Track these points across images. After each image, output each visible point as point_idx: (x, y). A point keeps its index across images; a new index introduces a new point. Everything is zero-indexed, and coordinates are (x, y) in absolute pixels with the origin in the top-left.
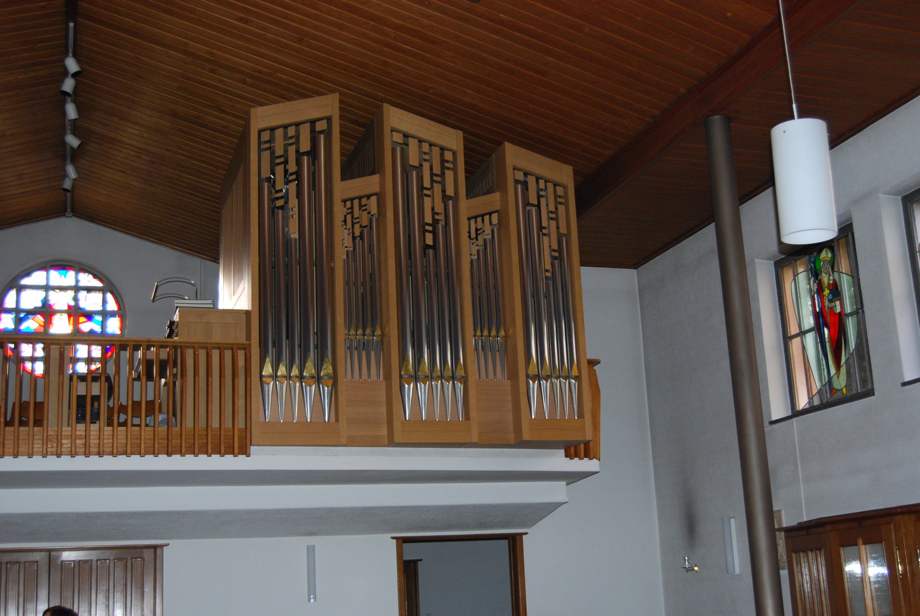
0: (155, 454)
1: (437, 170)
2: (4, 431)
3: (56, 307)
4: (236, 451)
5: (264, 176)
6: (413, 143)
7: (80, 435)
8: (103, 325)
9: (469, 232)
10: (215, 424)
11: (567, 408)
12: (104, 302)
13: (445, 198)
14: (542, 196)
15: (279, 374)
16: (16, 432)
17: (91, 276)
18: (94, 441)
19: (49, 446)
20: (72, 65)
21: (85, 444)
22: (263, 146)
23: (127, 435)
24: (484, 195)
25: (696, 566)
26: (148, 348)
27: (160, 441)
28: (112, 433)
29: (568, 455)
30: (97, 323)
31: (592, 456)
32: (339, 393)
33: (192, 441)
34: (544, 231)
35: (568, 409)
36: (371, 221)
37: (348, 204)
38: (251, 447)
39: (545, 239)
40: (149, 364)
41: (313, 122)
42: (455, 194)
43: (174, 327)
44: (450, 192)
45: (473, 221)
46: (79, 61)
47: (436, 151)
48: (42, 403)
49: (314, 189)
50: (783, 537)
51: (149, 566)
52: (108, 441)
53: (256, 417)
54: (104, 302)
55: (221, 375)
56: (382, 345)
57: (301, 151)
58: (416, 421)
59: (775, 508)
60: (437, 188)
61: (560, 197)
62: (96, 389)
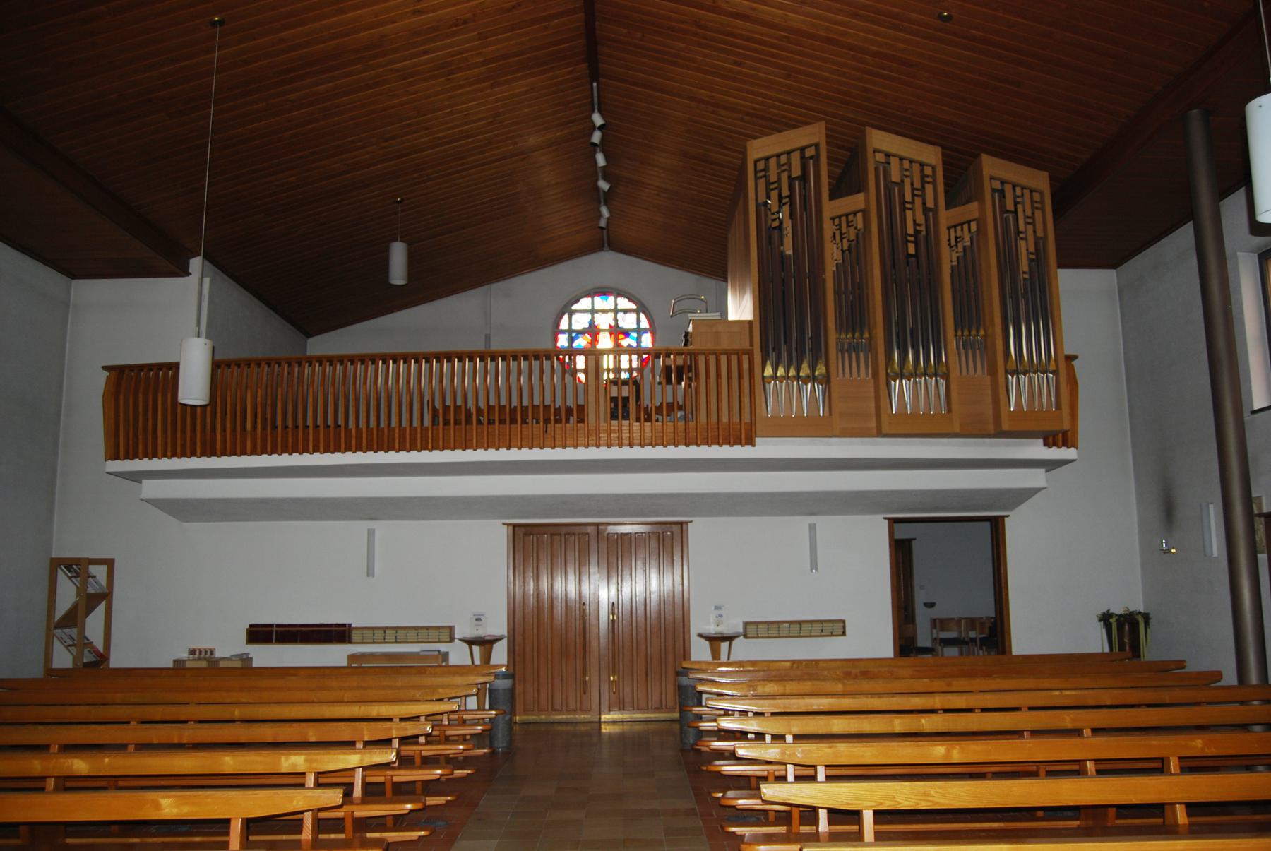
0: (676, 445)
1: (917, 185)
2: (554, 426)
3: (601, 328)
4: (743, 442)
5: (760, 201)
6: (895, 162)
7: (614, 430)
8: (639, 340)
9: (949, 240)
10: (725, 419)
11: (1045, 401)
12: (638, 321)
13: (926, 210)
14: (1019, 203)
15: (779, 374)
16: (564, 428)
17: (626, 300)
18: (626, 435)
19: (590, 439)
20: (598, 119)
21: (619, 438)
22: (759, 175)
23: (652, 429)
24: (963, 205)
25: (1173, 548)
26: (668, 356)
27: (668, 434)
28: (717, 426)
29: (1046, 444)
30: (633, 338)
31: (1070, 444)
32: (832, 390)
33: (706, 434)
34: (1021, 235)
35: (1046, 401)
36: (857, 235)
37: (837, 221)
38: (757, 439)
39: (1023, 243)
40: (667, 370)
41: (802, 150)
42: (935, 205)
43: (689, 337)
44: (930, 204)
45: (952, 231)
46: (603, 116)
47: (916, 167)
48: (583, 406)
49: (805, 210)
50: (1263, 522)
51: (677, 537)
52: (637, 435)
53: (760, 411)
54: (638, 321)
55: (729, 377)
56: (870, 347)
57: (793, 176)
58: (902, 413)
59: (1254, 495)
60: (918, 201)
61: (1036, 202)
62: (625, 391)
